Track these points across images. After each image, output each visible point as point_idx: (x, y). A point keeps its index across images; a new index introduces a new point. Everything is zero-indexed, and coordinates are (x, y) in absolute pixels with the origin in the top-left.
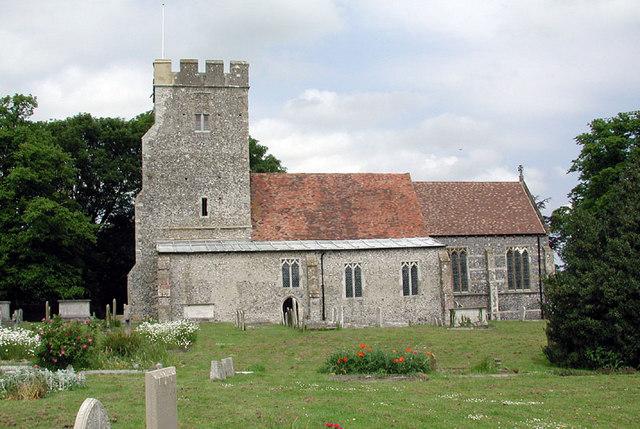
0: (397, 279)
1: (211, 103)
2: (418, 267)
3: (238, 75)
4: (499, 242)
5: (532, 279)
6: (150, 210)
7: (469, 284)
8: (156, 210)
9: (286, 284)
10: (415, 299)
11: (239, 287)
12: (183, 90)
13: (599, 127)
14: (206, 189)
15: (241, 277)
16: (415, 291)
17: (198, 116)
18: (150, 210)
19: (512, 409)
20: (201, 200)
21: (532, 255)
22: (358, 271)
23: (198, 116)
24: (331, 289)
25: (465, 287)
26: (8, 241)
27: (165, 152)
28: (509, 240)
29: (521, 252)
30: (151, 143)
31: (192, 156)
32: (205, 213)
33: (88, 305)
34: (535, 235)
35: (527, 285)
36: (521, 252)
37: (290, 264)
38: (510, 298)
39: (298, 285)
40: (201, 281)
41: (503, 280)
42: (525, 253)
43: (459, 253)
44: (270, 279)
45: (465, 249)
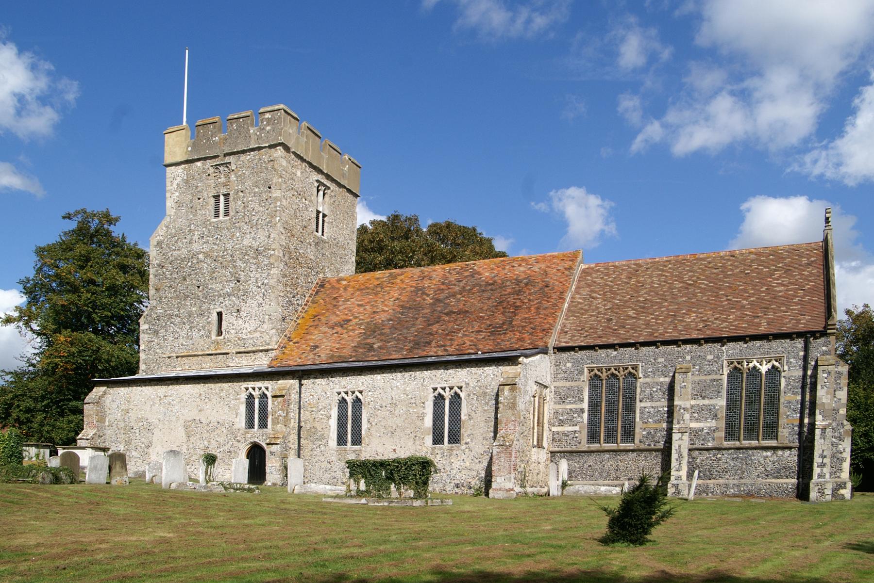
0: (421, 417)
1: (233, 177)
2: (462, 395)
3: (268, 128)
4: (709, 351)
5: (782, 421)
6: (156, 332)
7: (637, 430)
8: (162, 332)
9: (250, 424)
10: (451, 450)
11: (186, 427)
12: (199, 164)
13: (843, 136)
14: (221, 299)
15: (190, 414)
16: (455, 438)
17: (217, 197)
18: (156, 332)
19: (273, 522)
20: (215, 315)
21: (792, 372)
22: (357, 402)
23: (217, 197)
24: (313, 431)
25: (629, 434)
26: (768, 461)
27: (175, 253)
28: (731, 350)
29: (764, 368)
30: (159, 244)
31: (207, 255)
32: (220, 333)
33: (80, 465)
34: (800, 335)
35: (772, 430)
36: (764, 368)
37: (256, 393)
38: (725, 456)
39: (266, 426)
40: (140, 420)
41: (713, 424)
42: (774, 372)
43: (621, 374)
44: (225, 415)
45: (635, 368)
